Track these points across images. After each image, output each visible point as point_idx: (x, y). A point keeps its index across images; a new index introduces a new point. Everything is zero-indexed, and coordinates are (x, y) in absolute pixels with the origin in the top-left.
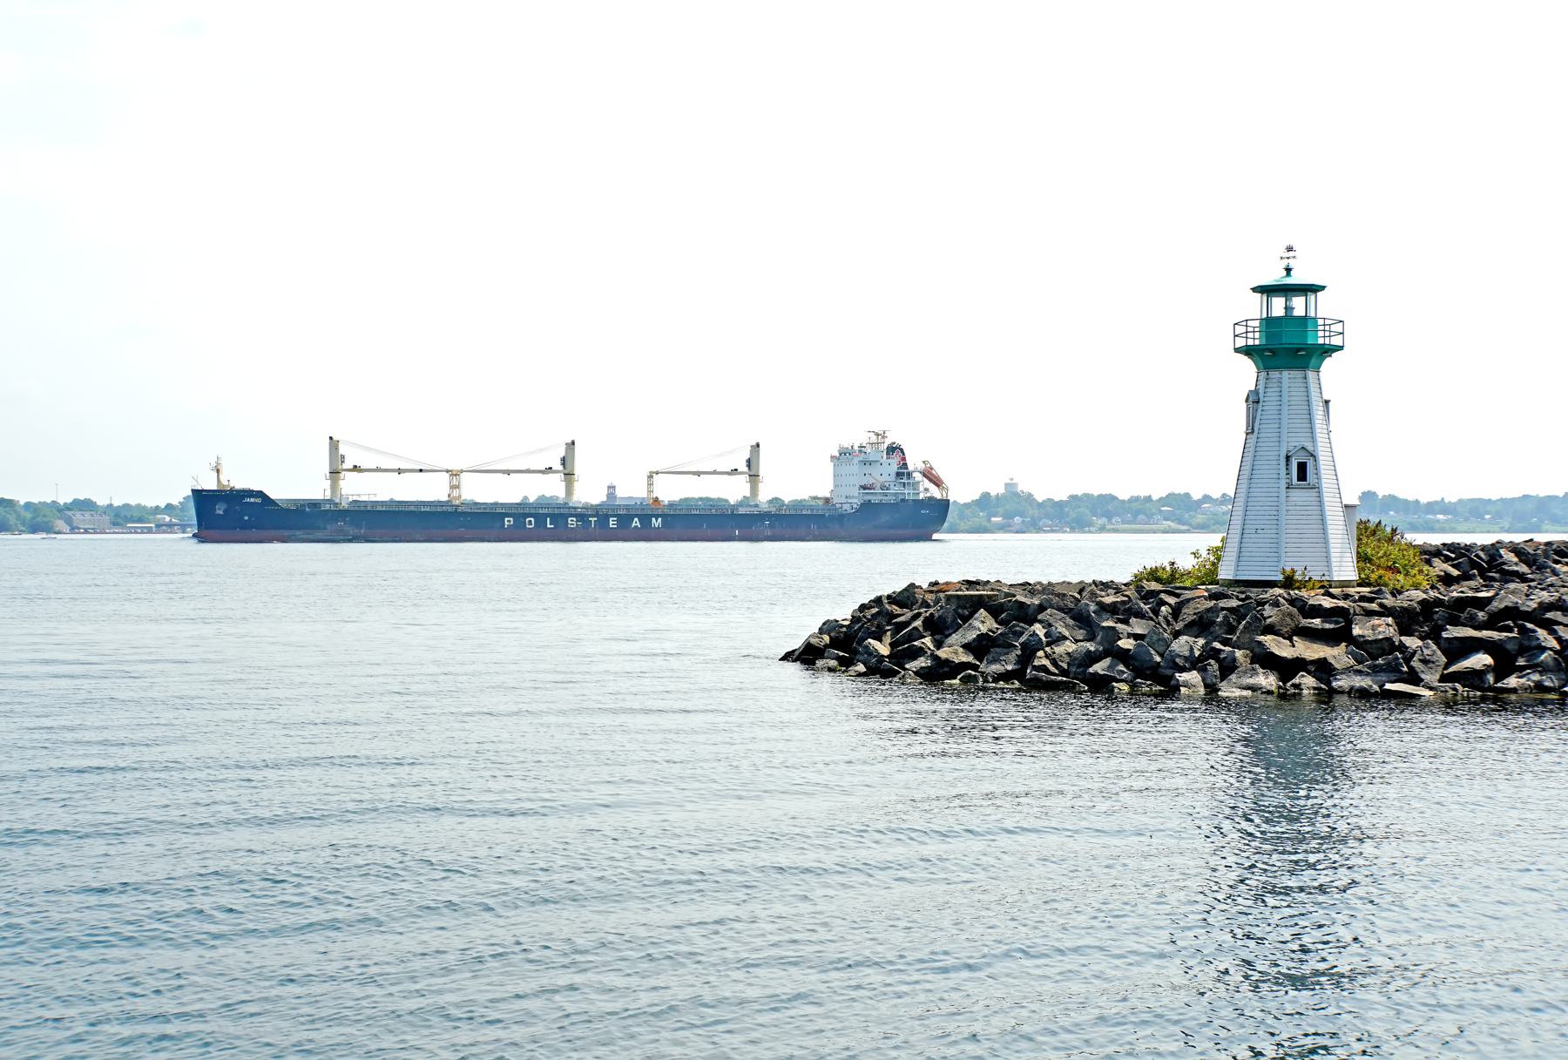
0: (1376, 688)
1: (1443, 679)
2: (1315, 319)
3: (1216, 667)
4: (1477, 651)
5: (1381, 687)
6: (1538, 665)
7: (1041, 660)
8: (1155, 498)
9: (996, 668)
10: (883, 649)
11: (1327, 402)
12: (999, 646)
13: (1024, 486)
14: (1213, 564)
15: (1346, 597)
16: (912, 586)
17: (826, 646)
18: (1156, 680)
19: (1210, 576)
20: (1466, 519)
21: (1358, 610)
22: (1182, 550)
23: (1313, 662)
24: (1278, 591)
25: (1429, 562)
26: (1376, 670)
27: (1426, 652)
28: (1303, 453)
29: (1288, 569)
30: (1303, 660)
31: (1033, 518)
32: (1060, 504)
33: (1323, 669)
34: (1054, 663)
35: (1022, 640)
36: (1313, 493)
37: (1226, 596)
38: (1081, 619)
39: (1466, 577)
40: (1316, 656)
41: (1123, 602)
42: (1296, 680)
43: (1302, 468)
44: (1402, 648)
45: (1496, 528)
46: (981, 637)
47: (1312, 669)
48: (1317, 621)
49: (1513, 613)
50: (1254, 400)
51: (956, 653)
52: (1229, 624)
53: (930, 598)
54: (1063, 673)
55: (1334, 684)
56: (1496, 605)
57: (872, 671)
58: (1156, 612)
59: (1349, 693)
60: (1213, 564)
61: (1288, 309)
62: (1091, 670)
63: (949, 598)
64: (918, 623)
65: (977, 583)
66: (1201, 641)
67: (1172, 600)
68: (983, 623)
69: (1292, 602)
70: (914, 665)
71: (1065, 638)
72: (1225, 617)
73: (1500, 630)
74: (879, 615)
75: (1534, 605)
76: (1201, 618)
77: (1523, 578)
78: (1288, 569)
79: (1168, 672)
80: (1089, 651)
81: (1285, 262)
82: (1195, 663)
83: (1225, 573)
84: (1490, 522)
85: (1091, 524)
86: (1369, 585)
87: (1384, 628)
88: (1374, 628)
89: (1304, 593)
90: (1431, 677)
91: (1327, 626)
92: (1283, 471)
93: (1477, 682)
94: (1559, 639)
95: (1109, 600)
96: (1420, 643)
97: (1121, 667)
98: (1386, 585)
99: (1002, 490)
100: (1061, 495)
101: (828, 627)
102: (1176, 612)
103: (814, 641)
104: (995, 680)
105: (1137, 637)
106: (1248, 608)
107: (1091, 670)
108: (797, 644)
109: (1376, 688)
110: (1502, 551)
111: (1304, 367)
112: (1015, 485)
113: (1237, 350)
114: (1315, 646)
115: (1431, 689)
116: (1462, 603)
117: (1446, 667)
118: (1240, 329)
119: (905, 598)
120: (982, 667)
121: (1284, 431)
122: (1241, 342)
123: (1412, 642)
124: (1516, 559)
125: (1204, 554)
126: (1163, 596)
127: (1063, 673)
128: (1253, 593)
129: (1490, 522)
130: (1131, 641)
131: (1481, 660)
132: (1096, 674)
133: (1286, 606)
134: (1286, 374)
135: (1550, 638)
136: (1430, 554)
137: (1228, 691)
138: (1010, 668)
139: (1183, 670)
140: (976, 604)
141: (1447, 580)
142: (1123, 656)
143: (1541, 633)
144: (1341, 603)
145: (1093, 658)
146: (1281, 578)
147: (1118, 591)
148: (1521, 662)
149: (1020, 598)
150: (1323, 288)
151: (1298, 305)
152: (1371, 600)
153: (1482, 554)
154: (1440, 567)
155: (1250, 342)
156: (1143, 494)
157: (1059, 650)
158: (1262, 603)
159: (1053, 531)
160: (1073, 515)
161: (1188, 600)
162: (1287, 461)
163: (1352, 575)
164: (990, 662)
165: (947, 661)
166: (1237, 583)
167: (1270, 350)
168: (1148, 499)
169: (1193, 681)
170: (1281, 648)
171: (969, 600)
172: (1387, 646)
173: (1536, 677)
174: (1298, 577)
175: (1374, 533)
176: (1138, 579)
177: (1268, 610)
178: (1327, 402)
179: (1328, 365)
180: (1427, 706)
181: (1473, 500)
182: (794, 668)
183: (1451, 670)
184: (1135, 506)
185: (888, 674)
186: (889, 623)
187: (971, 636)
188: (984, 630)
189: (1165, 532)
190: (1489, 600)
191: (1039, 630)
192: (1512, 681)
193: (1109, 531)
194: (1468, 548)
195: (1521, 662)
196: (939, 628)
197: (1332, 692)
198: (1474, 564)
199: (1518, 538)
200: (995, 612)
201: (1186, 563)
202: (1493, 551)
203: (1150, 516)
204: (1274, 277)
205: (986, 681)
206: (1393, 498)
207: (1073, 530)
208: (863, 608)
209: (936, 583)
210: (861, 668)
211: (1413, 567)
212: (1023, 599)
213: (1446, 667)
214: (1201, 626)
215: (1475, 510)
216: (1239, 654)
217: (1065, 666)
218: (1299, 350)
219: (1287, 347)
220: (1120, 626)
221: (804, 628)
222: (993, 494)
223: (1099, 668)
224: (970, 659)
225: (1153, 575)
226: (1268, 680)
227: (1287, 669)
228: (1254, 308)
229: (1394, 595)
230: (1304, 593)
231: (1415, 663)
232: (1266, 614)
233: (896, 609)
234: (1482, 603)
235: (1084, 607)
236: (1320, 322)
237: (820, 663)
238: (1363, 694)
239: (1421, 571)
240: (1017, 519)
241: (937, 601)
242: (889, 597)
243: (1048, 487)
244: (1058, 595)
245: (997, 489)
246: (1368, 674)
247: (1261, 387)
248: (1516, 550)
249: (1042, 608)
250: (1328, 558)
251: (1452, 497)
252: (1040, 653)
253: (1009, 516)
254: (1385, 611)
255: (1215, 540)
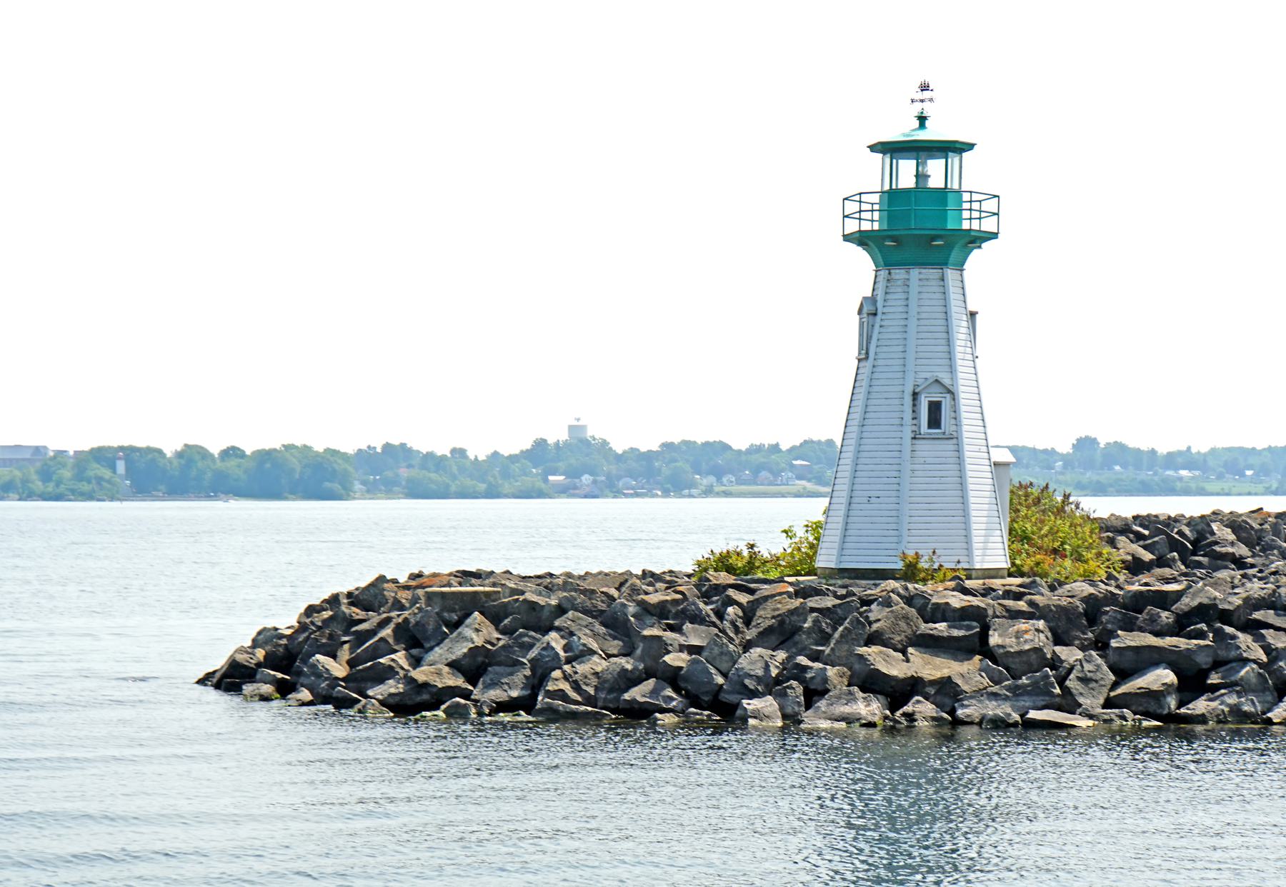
0: (1016, 717)
1: (1108, 704)
2: (959, 192)
3: (800, 690)
4: (1156, 664)
5: (1022, 716)
6: (1236, 684)
7: (556, 682)
8: (784, 447)
9: (496, 694)
10: (338, 669)
11: (973, 315)
12: (499, 664)
13: (595, 431)
14: (812, 546)
15: (987, 592)
16: (382, 579)
17: (259, 665)
18: (718, 709)
19: (803, 562)
20: (1220, 477)
21: (999, 610)
22: (767, 525)
23: (932, 683)
24: (892, 584)
25: (1112, 542)
26: (1017, 692)
27: (1087, 667)
28: (937, 388)
29: (911, 553)
30: (920, 679)
31: (609, 477)
32: (649, 456)
33: (946, 692)
34: (576, 687)
35: (533, 653)
36: (949, 446)
37: (818, 592)
38: (615, 624)
39: (1161, 562)
40: (938, 674)
41: (675, 602)
42: (908, 708)
43: (935, 408)
44: (1055, 663)
45: (1260, 488)
46: (474, 651)
47: (932, 691)
48: (942, 626)
49: (1207, 612)
50: (869, 311)
51: (439, 673)
52: (822, 631)
53: (404, 596)
54: (589, 700)
55: (960, 712)
56: (1187, 602)
57: (321, 698)
58: (720, 615)
59: (980, 724)
60: (812, 546)
61: (921, 177)
62: (627, 696)
63: (430, 597)
64: (387, 632)
65: (477, 575)
66: (781, 655)
67: (743, 598)
68: (478, 632)
69: (909, 600)
70: (378, 691)
71: (593, 652)
72: (816, 621)
73: (1190, 636)
74: (334, 621)
75: (1237, 601)
76: (782, 623)
77: (1239, 563)
78: (911, 553)
79: (732, 698)
80: (624, 670)
81: (917, 108)
82: (773, 686)
83: (825, 560)
84: (1252, 480)
85: (692, 485)
86: (1022, 575)
87: (1034, 634)
88: (1018, 635)
89: (928, 588)
90: (1092, 701)
91: (956, 633)
92: (908, 415)
93: (1152, 707)
94: (1267, 649)
95: (654, 599)
96: (1080, 655)
97: (669, 692)
98: (1044, 575)
99: (563, 436)
100: (650, 443)
101: (265, 637)
102: (748, 616)
103: (241, 658)
104: (494, 711)
105: (693, 650)
106: (847, 608)
107: (627, 696)
108: (218, 662)
109: (1016, 717)
110: (1215, 526)
111: (942, 264)
112: (583, 428)
113: (847, 238)
114: (938, 660)
115: (1091, 717)
116: (1138, 602)
117: (1115, 686)
118: (852, 207)
119: (369, 598)
120: (477, 693)
121: (911, 356)
122: (852, 226)
123: (1070, 654)
124: (1232, 537)
125: (800, 532)
126: (731, 592)
127: (589, 700)
128: (861, 588)
129: (1252, 480)
130: (685, 656)
131: (1162, 677)
132: (634, 701)
133: (900, 606)
134: (915, 273)
135: (1255, 646)
136: (1116, 529)
137: (814, 720)
138: (515, 694)
139: (753, 694)
140: (469, 604)
141: (1136, 567)
142: (673, 678)
143: (1244, 639)
144: (976, 601)
145: (631, 680)
146: (900, 565)
147: (671, 585)
148: (1214, 679)
149: (530, 596)
150: (970, 146)
151: (935, 168)
152: (1018, 597)
153: (1187, 531)
154: (1128, 548)
155: (866, 226)
156: (768, 441)
157: (582, 668)
158: (867, 602)
159: (637, 495)
160: (666, 471)
161: (766, 598)
162: (913, 399)
163: (1003, 563)
164: (488, 687)
165: (426, 685)
166: (842, 572)
167: (893, 238)
168: (775, 448)
169: (767, 711)
170: (893, 666)
171: (458, 601)
172: (1036, 660)
173: (1232, 699)
174: (923, 564)
175: (1037, 501)
176: (703, 567)
177: (875, 611)
178: (973, 315)
179: (977, 260)
180: (1090, 739)
181: (1230, 450)
182: (211, 694)
183: (1120, 691)
184: (758, 458)
185: (342, 703)
186: (346, 633)
187: (461, 650)
188: (479, 641)
189: (798, 495)
190: (1179, 595)
191: (555, 641)
192: (1200, 706)
193: (718, 495)
194: (1171, 521)
195: (1214, 679)
196: (415, 641)
197: (957, 722)
198: (1174, 545)
199: (1241, 505)
200: (495, 618)
201: (772, 545)
202: (1202, 526)
203: (776, 473)
204: (901, 129)
205: (480, 714)
206: (1120, 447)
207: (666, 494)
208: (311, 610)
209: (420, 575)
210: (305, 695)
211: (1089, 548)
212: (534, 598)
213: (1115, 686)
214: (783, 633)
215: (1231, 466)
216: (831, 672)
217: (591, 691)
218: (934, 238)
219: (918, 235)
220: (669, 636)
221: (231, 638)
222: (551, 441)
223: (638, 694)
224: (459, 682)
225: (724, 562)
226: (870, 708)
227: (897, 693)
228: (871, 175)
229: (1052, 588)
230: (928, 588)
231: (1071, 683)
232: (872, 617)
233: (357, 613)
234: (1164, 600)
235: (622, 609)
236: (966, 197)
237: (248, 688)
238: (999, 724)
239: (1099, 554)
240: (586, 479)
241: (414, 601)
242: (349, 595)
243: (631, 432)
244: (584, 592)
245: (557, 434)
246: (1006, 698)
247: (880, 293)
248: (1236, 524)
249: (561, 610)
250: (967, 538)
251: (1201, 446)
252: (557, 674)
253: (573, 473)
254: (1036, 612)
255: (814, 509)
